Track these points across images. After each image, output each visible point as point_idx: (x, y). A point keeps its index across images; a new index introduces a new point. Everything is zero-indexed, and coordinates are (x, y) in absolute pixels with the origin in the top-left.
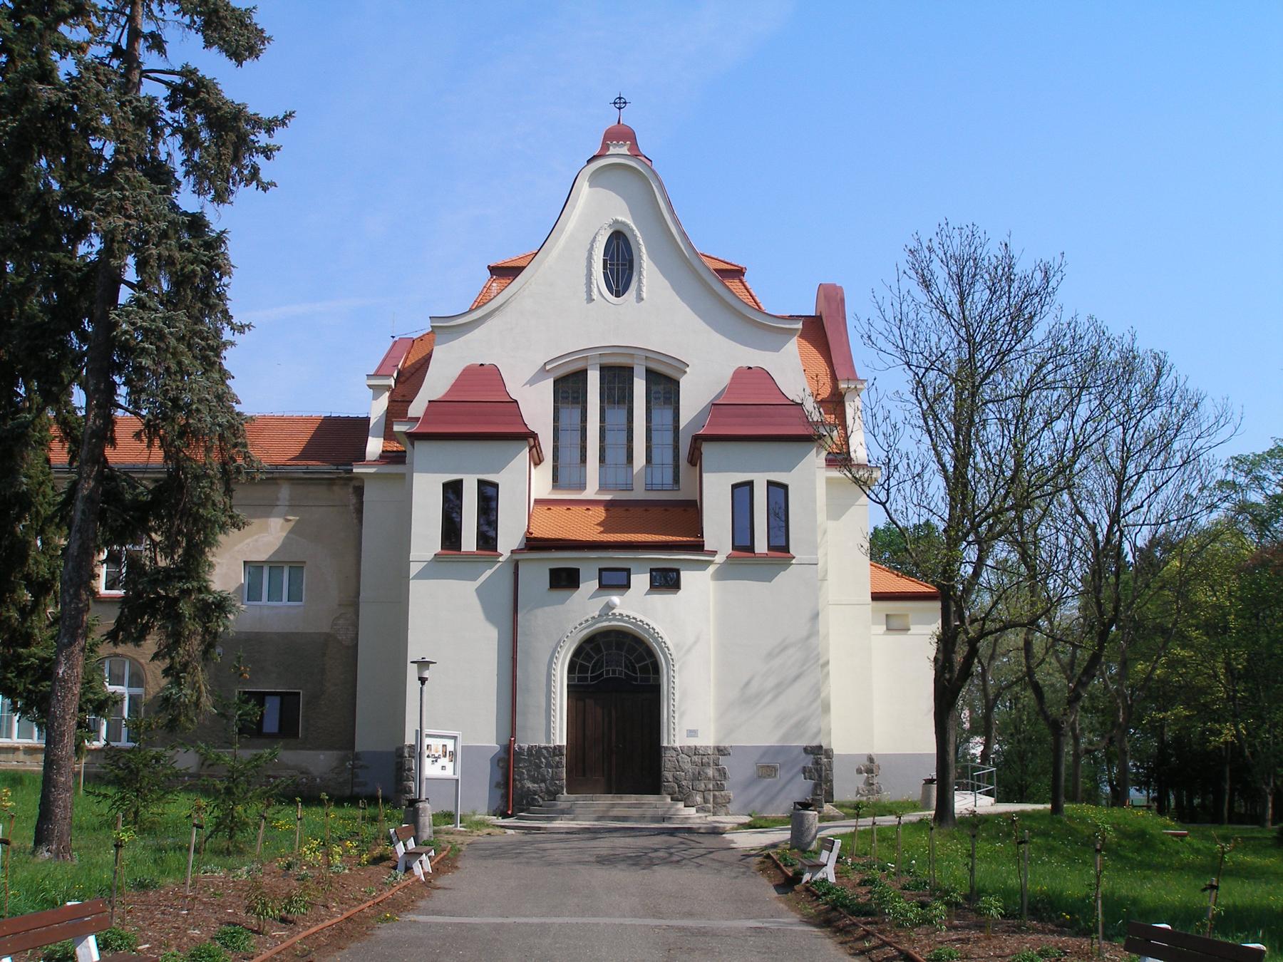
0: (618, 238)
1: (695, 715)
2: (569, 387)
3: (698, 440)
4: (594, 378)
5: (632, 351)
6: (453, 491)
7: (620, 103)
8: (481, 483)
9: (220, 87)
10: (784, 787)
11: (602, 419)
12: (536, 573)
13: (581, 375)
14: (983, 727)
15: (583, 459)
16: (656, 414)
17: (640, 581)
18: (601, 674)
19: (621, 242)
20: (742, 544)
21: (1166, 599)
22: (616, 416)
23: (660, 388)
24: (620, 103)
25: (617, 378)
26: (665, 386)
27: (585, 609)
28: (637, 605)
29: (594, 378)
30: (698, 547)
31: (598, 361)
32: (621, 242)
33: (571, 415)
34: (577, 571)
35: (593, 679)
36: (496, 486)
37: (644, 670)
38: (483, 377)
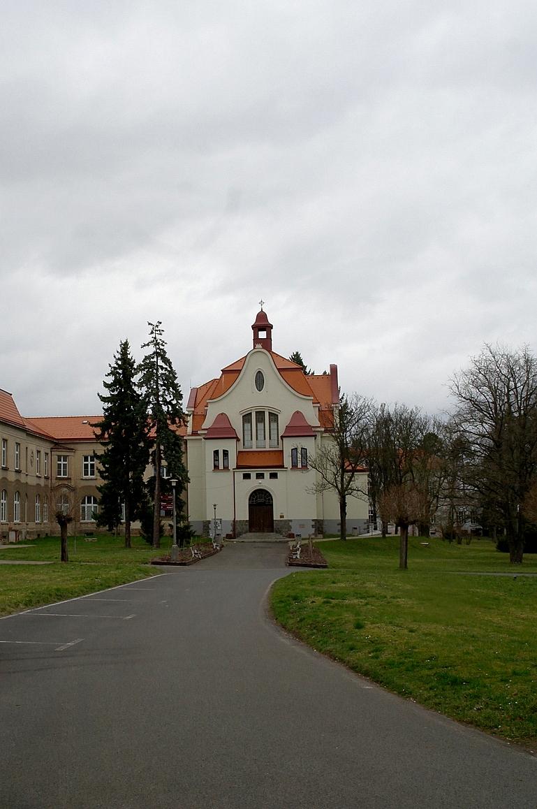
1: (280, 511)
2: (247, 418)
4: (89, 458)
6: (216, 453)
7: (262, 303)
8: (224, 451)
10: (270, 542)
14: (415, 449)
17: (267, 475)
20: (294, 466)
22: (261, 426)
24: (262, 303)
25: (260, 414)
26: (274, 417)
27: (254, 484)
28: (266, 483)
29: (89, 458)
30: (282, 467)
33: (247, 426)
38: (222, 417)
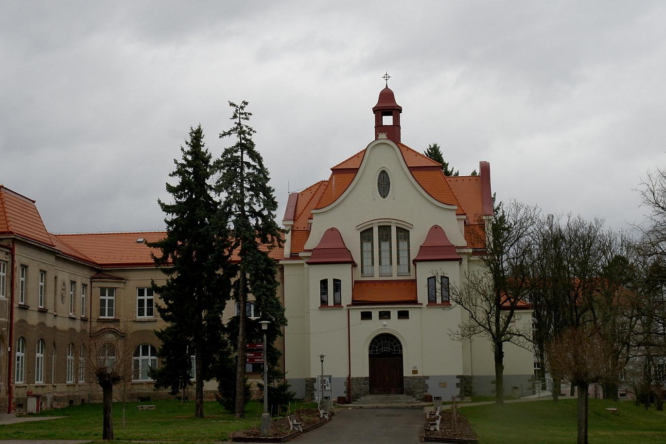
0: (383, 173)
1: (413, 363)
3: (415, 261)
5: (390, 221)
7: (387, 77)
9: (277, 209)
11: (380, 247)
12: (356, 314)
13: (371, 230)
15: (373, 264)
16: (401, 244)
17: (394, 314)
18: (381, 350)
19: (385, 175)
20: (432, 302)
21: (137, 390)
23: (402, 234)
25: (385, 230)
26: (404, 233)
27: (376, 326)
30: (415, 302)
31: (377, 225)
32: (385, 175)
33: (367, 246)
34: (371, 312)
35: (378, 352)
36: (340, 281)
37: (397, 348)
38: (333, 233)
